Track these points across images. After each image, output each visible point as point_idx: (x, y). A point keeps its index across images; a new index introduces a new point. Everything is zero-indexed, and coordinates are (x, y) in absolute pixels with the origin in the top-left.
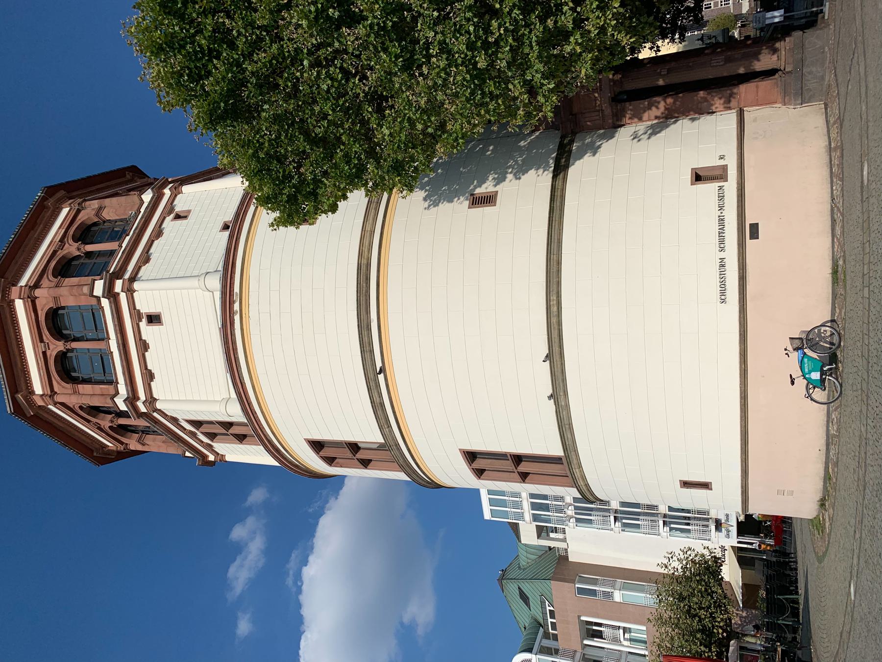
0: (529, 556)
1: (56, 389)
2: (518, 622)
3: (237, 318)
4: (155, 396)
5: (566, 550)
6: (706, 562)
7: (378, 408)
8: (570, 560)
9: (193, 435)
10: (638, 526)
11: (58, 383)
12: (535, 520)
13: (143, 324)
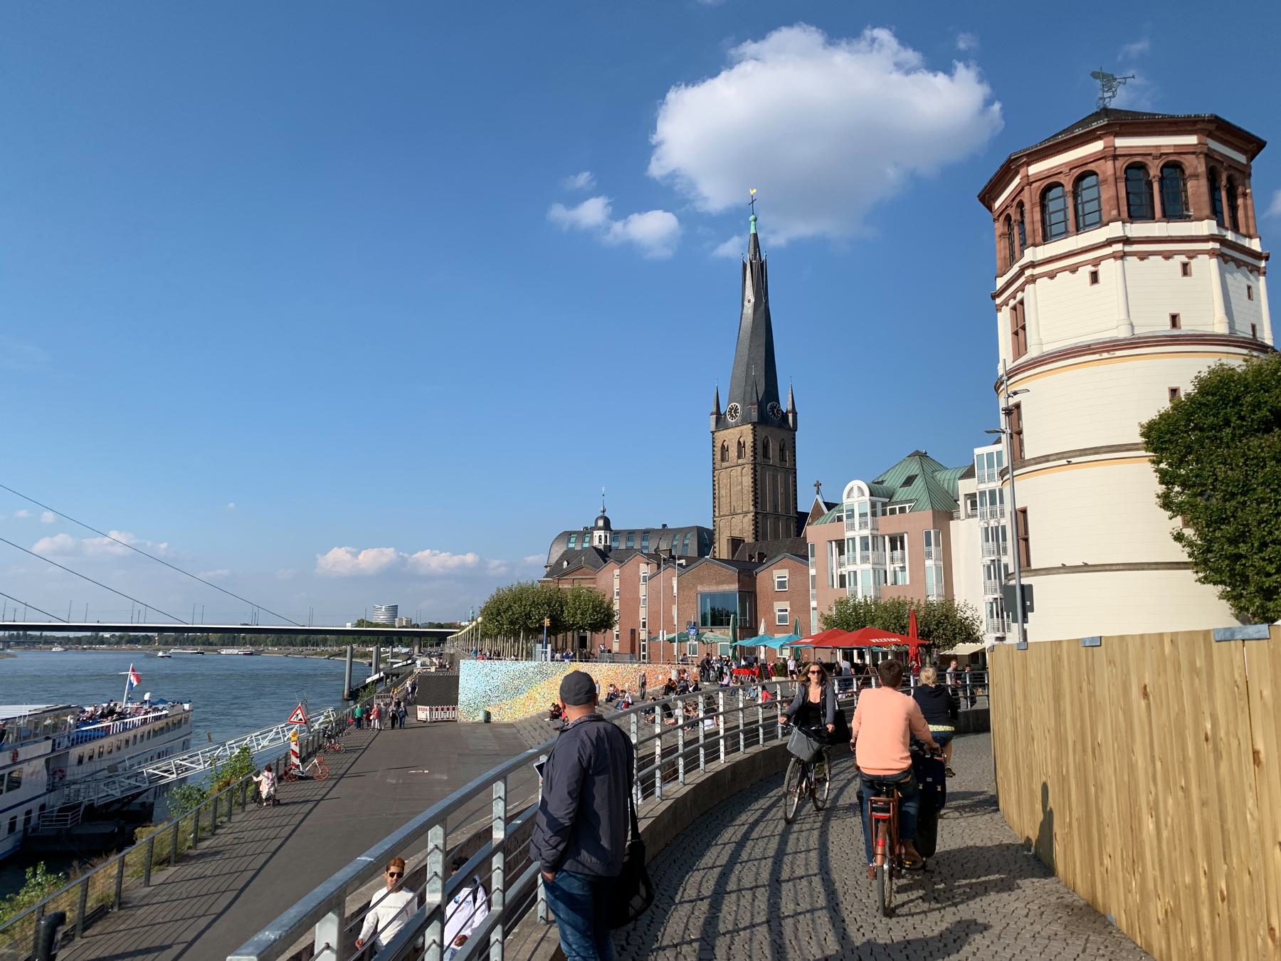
0: (946, 482)
1: (1034, 185)
2: (885, 473)
3: (1097, 357)
4: (1038, 281)
5: (959, 518)
6: (974, 633)
7: (1046, 458)
10: (990, 578)
12: (980, 493)
13: (1090, 268)
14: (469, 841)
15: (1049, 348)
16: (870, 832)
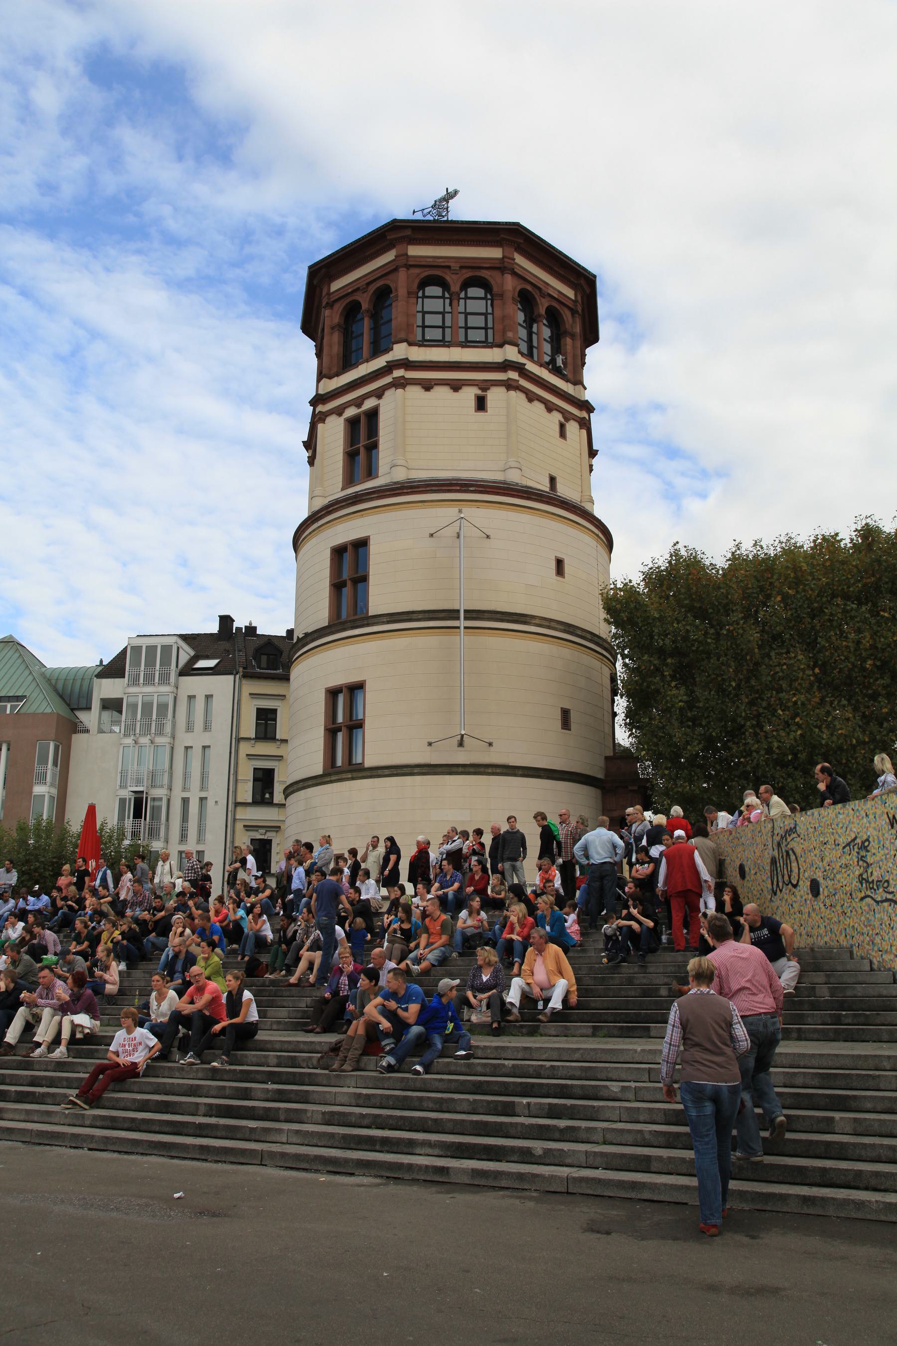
8: (73, 735)
9: (358, 403)
11: (419, 274)
14: (682, 1186)
15: (400, 475)
16: (830, 1064)
